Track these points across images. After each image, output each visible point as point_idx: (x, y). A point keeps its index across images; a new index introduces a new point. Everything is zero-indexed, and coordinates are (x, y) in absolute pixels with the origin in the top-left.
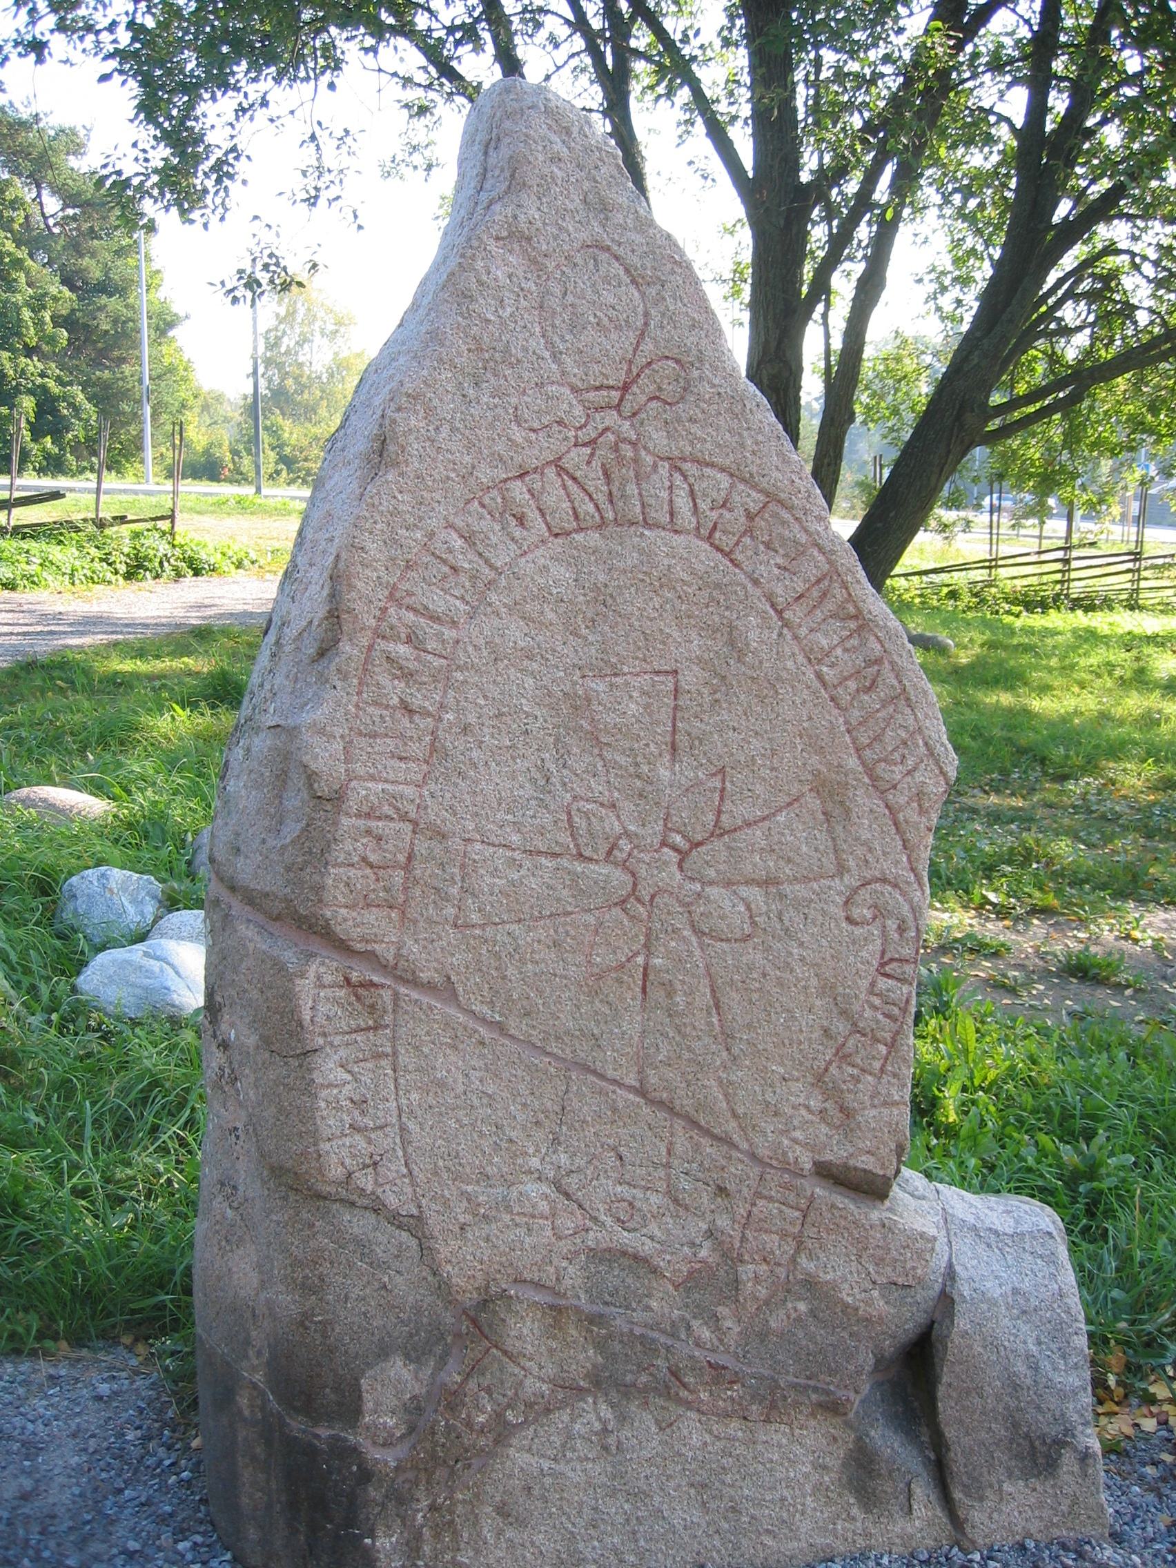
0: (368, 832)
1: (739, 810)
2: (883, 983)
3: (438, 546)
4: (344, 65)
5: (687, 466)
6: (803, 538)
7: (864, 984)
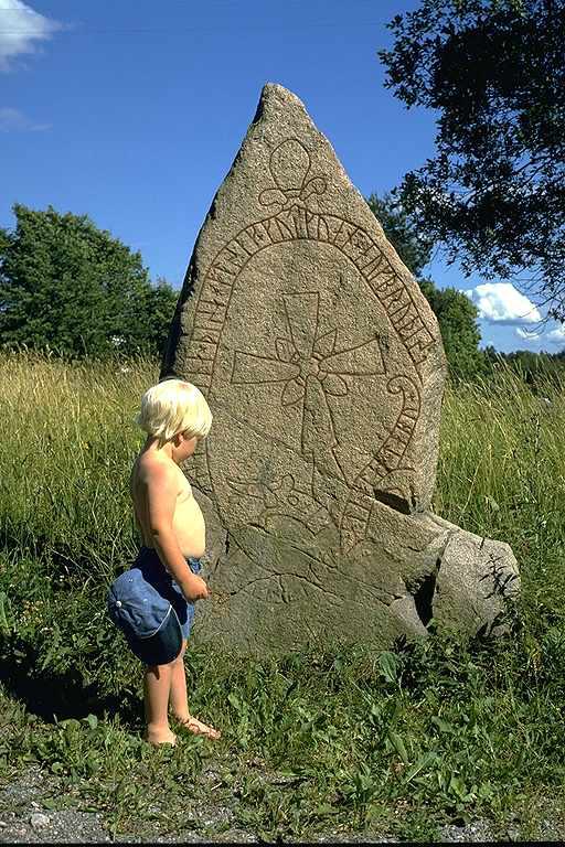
3: (229, 246)
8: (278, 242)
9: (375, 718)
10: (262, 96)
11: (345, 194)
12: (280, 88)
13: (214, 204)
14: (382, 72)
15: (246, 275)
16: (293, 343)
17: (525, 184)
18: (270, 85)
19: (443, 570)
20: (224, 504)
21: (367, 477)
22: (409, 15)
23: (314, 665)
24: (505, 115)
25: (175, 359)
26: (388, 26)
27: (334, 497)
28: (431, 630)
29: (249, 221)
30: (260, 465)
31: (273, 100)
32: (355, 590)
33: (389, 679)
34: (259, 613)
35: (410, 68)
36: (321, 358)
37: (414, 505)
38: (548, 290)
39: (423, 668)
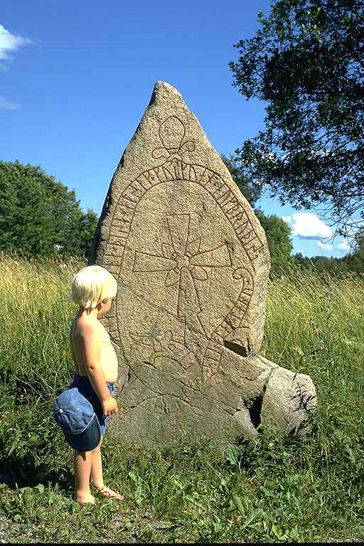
0: (114, 248)
1: (204, 248)
2: (243, 294)
3: (133, 184)
5: (194, 166)
6: (222, 182)
9: (223, 487)
10: (155, 89)
12: (166, 84)
13: (123, 157)
14: (231, 77)
15: (143, 203)
19: (268, 392)
21: (219, 333)
22: (247, 41)
24: (308, 106)
28: (260, 431)
29: (145, 168)
31: (161, 91)
32: (211, 406)
33: (232, 463)
35: (249, 73)
37: (250, 351)
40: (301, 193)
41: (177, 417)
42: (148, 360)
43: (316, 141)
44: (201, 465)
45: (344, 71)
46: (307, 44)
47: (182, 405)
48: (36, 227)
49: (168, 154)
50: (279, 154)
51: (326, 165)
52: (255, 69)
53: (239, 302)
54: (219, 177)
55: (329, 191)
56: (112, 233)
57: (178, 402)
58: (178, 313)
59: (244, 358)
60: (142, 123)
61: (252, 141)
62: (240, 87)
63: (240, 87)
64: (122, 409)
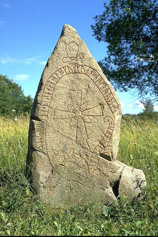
1: (89, 107)
3: (53, 75)
4: (108, 50)
6: (98, 74)
7: (106, 130)
8: (69, 74)
9: (103, 229)
10: (63, 28)
11: (90, 59)
12: (69, 26)
13: (48, 62)
14: (92, 32)
15: (58, 85)
16: (73, 106)
17: (133, 64)
18: (66, 25)
19: (122, 179)
20: (51, 158)
21: (97, 149)
22: (99, 16)
23: (81, 210)
24: (126, 45)
25: (35, 111)
26: (93, 18)
27: (87, 155)
28: (119, 198)
29: (59, 67)
30: (63, 145)
31: (67, 29)
32: (94, 186)
33: (106, 215)
34: (62, 193)
35: (99, 31)
36: (82, 111)
37: (112, 158)
38: (140, 95)
39: (117, 211)
40: (123, 85)
41: (77, 192)
42: (61, 163)
43: (130, 61)
44: (90, 216)
45: (141, 30)
46: (125, 18)
47: (79, 186)
48: (4, 102)
49: (70, 60)
50: (114, 67)
51: (134, 72)
52: (103, 29)
53: (107, 133)
54: (96, 71)
55: (136, 83)
56: (43, 100)
57: (77, 184)
58: (76, 139)
59: (110, 162)
60: (57, 45)
61: (101, 61)
62: (96, 36)
63: (96, 36)
64: (49, 188)
